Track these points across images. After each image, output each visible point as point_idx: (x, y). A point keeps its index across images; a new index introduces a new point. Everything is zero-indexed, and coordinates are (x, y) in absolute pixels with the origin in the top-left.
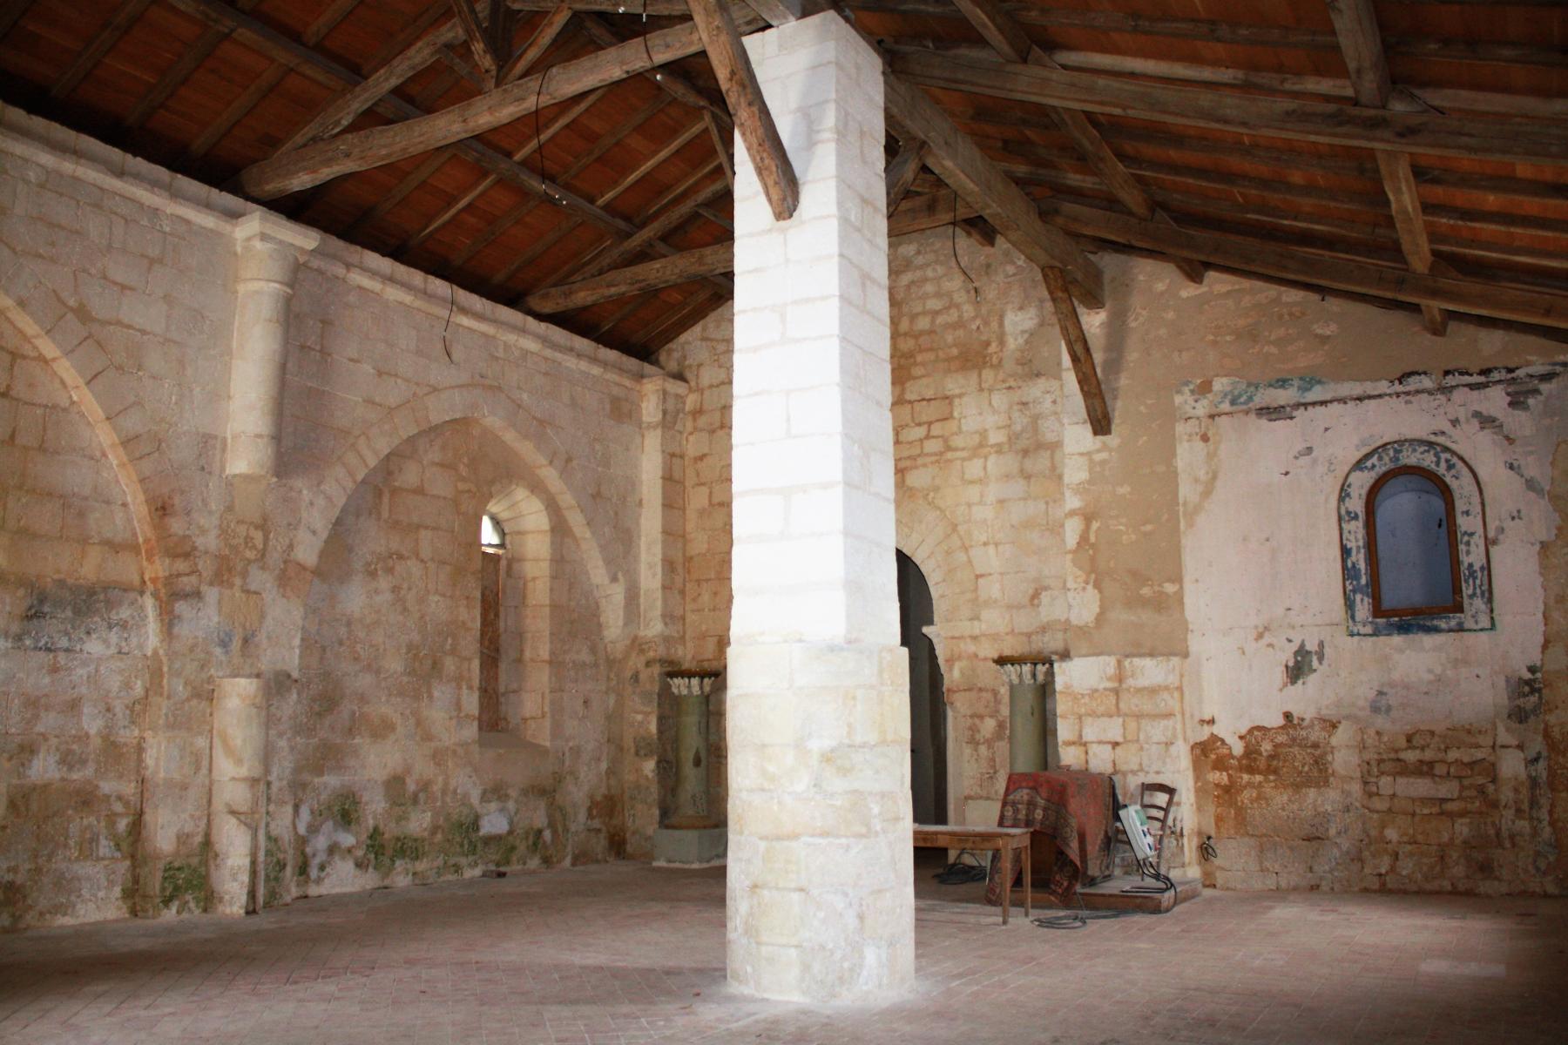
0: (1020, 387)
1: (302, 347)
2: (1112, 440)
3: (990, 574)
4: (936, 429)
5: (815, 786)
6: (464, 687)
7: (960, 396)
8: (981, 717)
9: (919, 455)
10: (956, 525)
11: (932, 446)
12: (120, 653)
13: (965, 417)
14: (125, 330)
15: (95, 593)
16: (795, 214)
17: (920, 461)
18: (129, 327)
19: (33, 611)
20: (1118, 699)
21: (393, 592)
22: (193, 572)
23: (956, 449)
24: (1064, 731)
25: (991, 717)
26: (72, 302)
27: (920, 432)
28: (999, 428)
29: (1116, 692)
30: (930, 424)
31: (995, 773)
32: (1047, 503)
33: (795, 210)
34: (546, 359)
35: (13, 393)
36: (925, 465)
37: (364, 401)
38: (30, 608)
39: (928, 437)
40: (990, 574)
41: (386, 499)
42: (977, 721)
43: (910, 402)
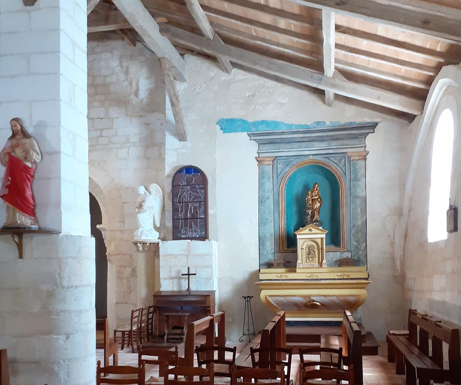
4: (105, 133)
7: (117, 118)
8: (124, 267)
23: (115, 143)
24: (163, 273)
29: (187, 256)
30: (102, 130)
31: (130, 292)
39: (101, 136)
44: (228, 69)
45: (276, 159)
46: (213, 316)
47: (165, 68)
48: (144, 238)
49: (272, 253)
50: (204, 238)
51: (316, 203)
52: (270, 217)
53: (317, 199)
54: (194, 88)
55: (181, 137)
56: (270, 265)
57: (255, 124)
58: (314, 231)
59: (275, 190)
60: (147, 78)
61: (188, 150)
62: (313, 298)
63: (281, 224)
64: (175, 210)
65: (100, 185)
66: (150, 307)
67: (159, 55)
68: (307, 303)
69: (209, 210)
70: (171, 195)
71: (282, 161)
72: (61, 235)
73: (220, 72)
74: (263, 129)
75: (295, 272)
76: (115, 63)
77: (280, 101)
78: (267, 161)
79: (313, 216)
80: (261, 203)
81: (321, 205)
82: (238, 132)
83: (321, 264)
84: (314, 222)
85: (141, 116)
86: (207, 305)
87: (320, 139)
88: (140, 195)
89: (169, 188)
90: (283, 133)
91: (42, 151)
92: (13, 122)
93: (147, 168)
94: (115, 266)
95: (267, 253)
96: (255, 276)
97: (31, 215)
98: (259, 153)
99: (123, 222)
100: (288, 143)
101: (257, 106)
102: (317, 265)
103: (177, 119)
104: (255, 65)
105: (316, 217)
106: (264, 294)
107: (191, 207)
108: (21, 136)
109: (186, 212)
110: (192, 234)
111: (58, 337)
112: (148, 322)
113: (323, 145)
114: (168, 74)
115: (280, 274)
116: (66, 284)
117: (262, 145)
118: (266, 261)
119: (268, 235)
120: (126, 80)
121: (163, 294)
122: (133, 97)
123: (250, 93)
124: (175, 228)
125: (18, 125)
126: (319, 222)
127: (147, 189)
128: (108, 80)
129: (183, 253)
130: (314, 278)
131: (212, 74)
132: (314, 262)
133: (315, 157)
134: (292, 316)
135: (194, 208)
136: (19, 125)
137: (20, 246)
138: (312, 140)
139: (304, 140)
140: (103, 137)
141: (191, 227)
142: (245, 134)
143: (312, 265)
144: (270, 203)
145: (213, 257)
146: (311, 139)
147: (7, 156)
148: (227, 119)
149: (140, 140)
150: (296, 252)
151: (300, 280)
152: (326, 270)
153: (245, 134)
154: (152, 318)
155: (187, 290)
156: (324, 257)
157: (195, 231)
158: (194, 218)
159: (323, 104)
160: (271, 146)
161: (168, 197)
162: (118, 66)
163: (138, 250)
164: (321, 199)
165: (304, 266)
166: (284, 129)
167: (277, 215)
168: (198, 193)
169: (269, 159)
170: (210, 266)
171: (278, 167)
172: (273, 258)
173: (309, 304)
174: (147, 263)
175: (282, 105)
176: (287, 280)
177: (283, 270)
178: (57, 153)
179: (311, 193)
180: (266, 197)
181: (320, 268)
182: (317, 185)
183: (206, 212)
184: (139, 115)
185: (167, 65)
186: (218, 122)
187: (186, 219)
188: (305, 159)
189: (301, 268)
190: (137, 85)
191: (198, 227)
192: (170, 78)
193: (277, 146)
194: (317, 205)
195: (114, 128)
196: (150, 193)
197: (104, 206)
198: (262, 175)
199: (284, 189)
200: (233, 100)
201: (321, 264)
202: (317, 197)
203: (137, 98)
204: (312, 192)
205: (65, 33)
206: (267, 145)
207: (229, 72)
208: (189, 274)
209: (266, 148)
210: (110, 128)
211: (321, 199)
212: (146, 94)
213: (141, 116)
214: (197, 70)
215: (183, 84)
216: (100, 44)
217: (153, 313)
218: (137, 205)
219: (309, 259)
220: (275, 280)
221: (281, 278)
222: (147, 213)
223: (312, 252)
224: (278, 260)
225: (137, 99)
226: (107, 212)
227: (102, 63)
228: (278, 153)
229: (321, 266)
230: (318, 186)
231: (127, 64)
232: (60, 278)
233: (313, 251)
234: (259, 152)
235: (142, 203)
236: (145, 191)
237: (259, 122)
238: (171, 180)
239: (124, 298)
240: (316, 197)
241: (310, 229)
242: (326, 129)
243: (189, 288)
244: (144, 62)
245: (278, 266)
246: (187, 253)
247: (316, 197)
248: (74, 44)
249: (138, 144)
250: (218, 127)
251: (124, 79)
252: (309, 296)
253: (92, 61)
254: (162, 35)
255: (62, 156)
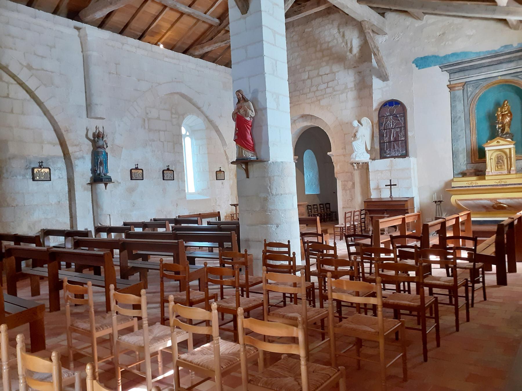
0: (358, 67)
1: (110, 73)
2: (390, 83)
3: (349, 133)
4: (330, 84)
5: (262, 208)
6: (180, 181)
7: (338, 72)
8: (347, 181)
9: (324, 94)
10: (337, 118)
11: (329, 90)
12: (59, 178)
13: (340, 79)
14: (45, 72)
15: (48, 160)
16: (248, 12)
17: (325, 96)
18: (47, 71)
19: (28, 167)
20: (391, 174)
21: (152, 152)
22: (80, 151)
23: (337, 91)
24: (373, 185)
25: (350, 181)
26: (25, 64)
27: (325, 86)
28: (351, 82)
29: (390, 171)
30: (328, 83)
31: (352, 199)
32: (368, 107)
33: (248, 10)
34: (198, 71)
35: (10, 96)
36: (327, 98)
37: (134, 90)
38: (27, 166)
39: (327, 87)
40: (349, 133)
41: (146, 122)
42: (346, 183)
43: (321, 76)
44: (419, 17)
45: (466, 84)
46: (445, 219)
47: (365, 28)
48: (357, 160)
49: (465, 164)
50: (405, 155)
51: (506, 118)
52: (462, 134)
53: (507, 114)
54: (393, 38)
55: (384, 77)
56: (464, 174)
57: (445, 57)
58: (502, 142)
59: (466, 110)
60: (358, 37)
61: (390, 88)
62: (498, 201)
63: (472, 140)
64: (381, 136)
65: (328, 124)
66: (362, 210)
67: (359, 19)
68: (494, 205)
69: (409, 133)
70: (378, 124)
71: (471, 85)
72: (269, 162)
73: (414, 20)
74: (453, 60)
75: (485, 179)
76: (335, 31)
77: (468, 34)
78: (458, 87)
79: (503, 130)
80: (453, 122)
81: (511, 119)
82: (431, 66)
83: (509, 172)
84: (505, 134)
85: (355, 67)
86: (406, 208)
87: (508, 60)
88: (354, 127)
89: (376, 120)
90: (472, 61)
91: (257, 108)
92: (237, 92)
93: (361, 106)
94: (340, 181)
95: (461, 165)
96: (448, 184)
97: (251, 151)
98: (450, 81)
99: (345, 149)
100: (476, 68)
101: (447, 42)
102: (506, 172)
103: (379, 65)
104: (434, 11)
105: (507, 129)
106: (454, 199)
107: (394, 132)
108: (243, 101)
109: (390, 136)
110: (395, 153)
111: (272, 226)
112: (361, 221)
113: (512, 65)
114: (368, 32)
115: (470, 182)
116: (274, 193)
117: (452, 74)
118: (459, 171)
119: (460, 149)
120: (343, 42)
121: (373, 200)
122: (348, 54)
123: (441, 33)
124: (382, 150)
125: (240, 94)
126: (510, 134)
127: (359, 122)
128: (330, 45)
129: (387, 169)
130: (503, 183)
131: (408, 23)
132: (503, 169)
133: (503, 78)
134: (482, 216)
135: (396, 132)
136: (241, 94)
137: (247, 171)
138: (500, 63)
139: (492, 64)
140: (329, 87)
141: (394, 148)
142: (437, 67)
143: (501, 172)
144: (462, 122)
145: (412, 171)
146: (499, 62)
147: (236, 115)
148: (421, 58)
149: (355, 85)
150: (485, 162)
151: (489, 186)
152: (514, 176)
153: (437, 67)
154: (365, 218)
155: (390, 197)
156: (512, 165)
157: (398, 151)
158: (396, 140)
159: (510, 29)
160: (461, 74)
161: (376, 126)
162: (337, 32)
163: (354, 169)
164: (511, 114)
165: (494, 174)
166: (474, 57)
167: (468, 132)
168: (399, 120)
169: (460, 85)
170: (410, 178)
171: (468, 91)
172: (466, 168)
173: (496, 206)
174: (361, 177)
175: (470, 37)
176: (476, 186)
177: (475, 178)
178: (266, 109)
179: (501, 109)
180: (458, 117)
181: (509, 175)
182: (506, 102)
183: (406, 135)
184: (354, 66)
185: (367, 26)
186: (414, 61)
187: (390, 142)
188: (494, 80)
189: (490, 176)
190: (351, 44)
191: (399, 147)
192: (370, 35)
193: (467, 73)
194: (508, 119)
195: (336, 80)
196: (361, 124)
197: (332, 138)
198: (453, 99)
199: (474, 109)
200: (426, 41)
201: (509, 172)
202: (507, 112)
203: (352, 54)
204: (502, 108)
205: (267, 27)
206: (457, 73)
207: (421, 19)
208: (391, 185)
209: (457, 76)
210: (334, 80)
211: (511, 114)
212: (358, 49)
213: (355, 67)
214: (395, 23)
215: (385, 36)
216: (324, 19)
217: (365, 214)
218: (353, 135)
219: (498, 167)
220: (466, 187)
221: (471, 185)
222: (360, 141)
223: (501, 161)
224: (471, 170)
225: (351, 55)
226: (334, 142)
227: (326, 33)
228: (469, 78)
229: (510, 173)
230: (507, 102)
231: (343, 30)
232: (270, 189)
233: (502, 160)
234: (450, 80)
235: (356, 133)
236: (358, 124)
237: (449, 55)
238: (377, 113)
239: (348, 204)
240: (505, 113)
241: (498, 141)
242: (514, 51)
243: (391, 195)
244: (355, 25)
245: (471, 175)
246: (391, 168)
247: (505, 113)
248: (275, 33)
249: (354, 89)
250: (414, 65)
251: (342, 41)
252: (495, 199)
253: (319, 32)
254: (360, 4)
255: (268, 110)
